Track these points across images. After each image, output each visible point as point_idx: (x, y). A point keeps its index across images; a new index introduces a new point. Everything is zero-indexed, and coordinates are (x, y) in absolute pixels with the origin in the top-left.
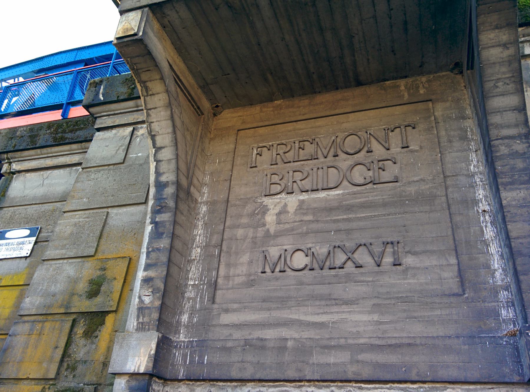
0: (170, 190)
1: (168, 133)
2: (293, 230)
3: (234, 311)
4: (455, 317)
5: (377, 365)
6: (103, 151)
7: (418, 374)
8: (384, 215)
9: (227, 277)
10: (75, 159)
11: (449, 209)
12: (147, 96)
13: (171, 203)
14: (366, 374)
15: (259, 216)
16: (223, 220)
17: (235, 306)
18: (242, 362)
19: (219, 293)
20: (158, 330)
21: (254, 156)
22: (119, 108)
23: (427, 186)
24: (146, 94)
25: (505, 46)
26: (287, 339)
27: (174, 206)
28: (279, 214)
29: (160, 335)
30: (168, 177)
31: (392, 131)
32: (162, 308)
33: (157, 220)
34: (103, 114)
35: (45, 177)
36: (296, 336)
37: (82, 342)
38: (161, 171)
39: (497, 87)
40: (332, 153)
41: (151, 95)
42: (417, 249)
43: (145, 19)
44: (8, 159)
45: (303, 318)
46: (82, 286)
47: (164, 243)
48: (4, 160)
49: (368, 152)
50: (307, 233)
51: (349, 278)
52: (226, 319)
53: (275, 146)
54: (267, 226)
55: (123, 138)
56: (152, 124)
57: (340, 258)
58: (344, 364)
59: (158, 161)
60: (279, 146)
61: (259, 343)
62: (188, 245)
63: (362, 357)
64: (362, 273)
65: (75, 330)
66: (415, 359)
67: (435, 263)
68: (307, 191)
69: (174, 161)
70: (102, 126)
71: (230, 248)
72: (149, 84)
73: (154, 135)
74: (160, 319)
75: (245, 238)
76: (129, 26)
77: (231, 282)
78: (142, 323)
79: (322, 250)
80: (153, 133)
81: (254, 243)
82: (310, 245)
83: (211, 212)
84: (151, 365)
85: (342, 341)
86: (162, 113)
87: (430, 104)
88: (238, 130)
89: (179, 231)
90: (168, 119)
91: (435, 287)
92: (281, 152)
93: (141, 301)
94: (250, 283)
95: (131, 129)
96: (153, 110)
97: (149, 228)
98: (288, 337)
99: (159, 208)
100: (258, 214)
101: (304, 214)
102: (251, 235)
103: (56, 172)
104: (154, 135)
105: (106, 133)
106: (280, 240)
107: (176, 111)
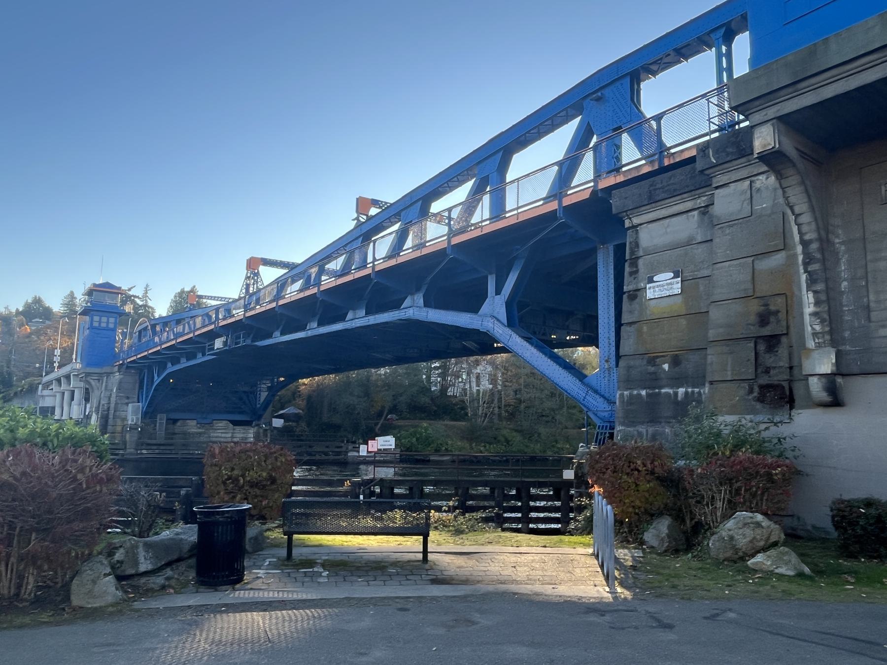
0: (814, 246)
12: (782, 179)
13: (818, 256)
22: (731, 166)
24: (779, 178)
32: (831, 332)
33: (809, 269)
34: (717, 173)
35: (666, 226)
37: (767, 356)
38: (804, 232)
44: (628, 215)
46: (753, 318)
55: (743, 192)
65: (758, 347)
69: (813, 223)
72: (783, 172)
78: (819, 343)
84: (834, 368)
86: (797, 189)
90: (803, 193)
93: (813, 329)
95: (747, 183)
97: (804, 277)
99: (808, 260)
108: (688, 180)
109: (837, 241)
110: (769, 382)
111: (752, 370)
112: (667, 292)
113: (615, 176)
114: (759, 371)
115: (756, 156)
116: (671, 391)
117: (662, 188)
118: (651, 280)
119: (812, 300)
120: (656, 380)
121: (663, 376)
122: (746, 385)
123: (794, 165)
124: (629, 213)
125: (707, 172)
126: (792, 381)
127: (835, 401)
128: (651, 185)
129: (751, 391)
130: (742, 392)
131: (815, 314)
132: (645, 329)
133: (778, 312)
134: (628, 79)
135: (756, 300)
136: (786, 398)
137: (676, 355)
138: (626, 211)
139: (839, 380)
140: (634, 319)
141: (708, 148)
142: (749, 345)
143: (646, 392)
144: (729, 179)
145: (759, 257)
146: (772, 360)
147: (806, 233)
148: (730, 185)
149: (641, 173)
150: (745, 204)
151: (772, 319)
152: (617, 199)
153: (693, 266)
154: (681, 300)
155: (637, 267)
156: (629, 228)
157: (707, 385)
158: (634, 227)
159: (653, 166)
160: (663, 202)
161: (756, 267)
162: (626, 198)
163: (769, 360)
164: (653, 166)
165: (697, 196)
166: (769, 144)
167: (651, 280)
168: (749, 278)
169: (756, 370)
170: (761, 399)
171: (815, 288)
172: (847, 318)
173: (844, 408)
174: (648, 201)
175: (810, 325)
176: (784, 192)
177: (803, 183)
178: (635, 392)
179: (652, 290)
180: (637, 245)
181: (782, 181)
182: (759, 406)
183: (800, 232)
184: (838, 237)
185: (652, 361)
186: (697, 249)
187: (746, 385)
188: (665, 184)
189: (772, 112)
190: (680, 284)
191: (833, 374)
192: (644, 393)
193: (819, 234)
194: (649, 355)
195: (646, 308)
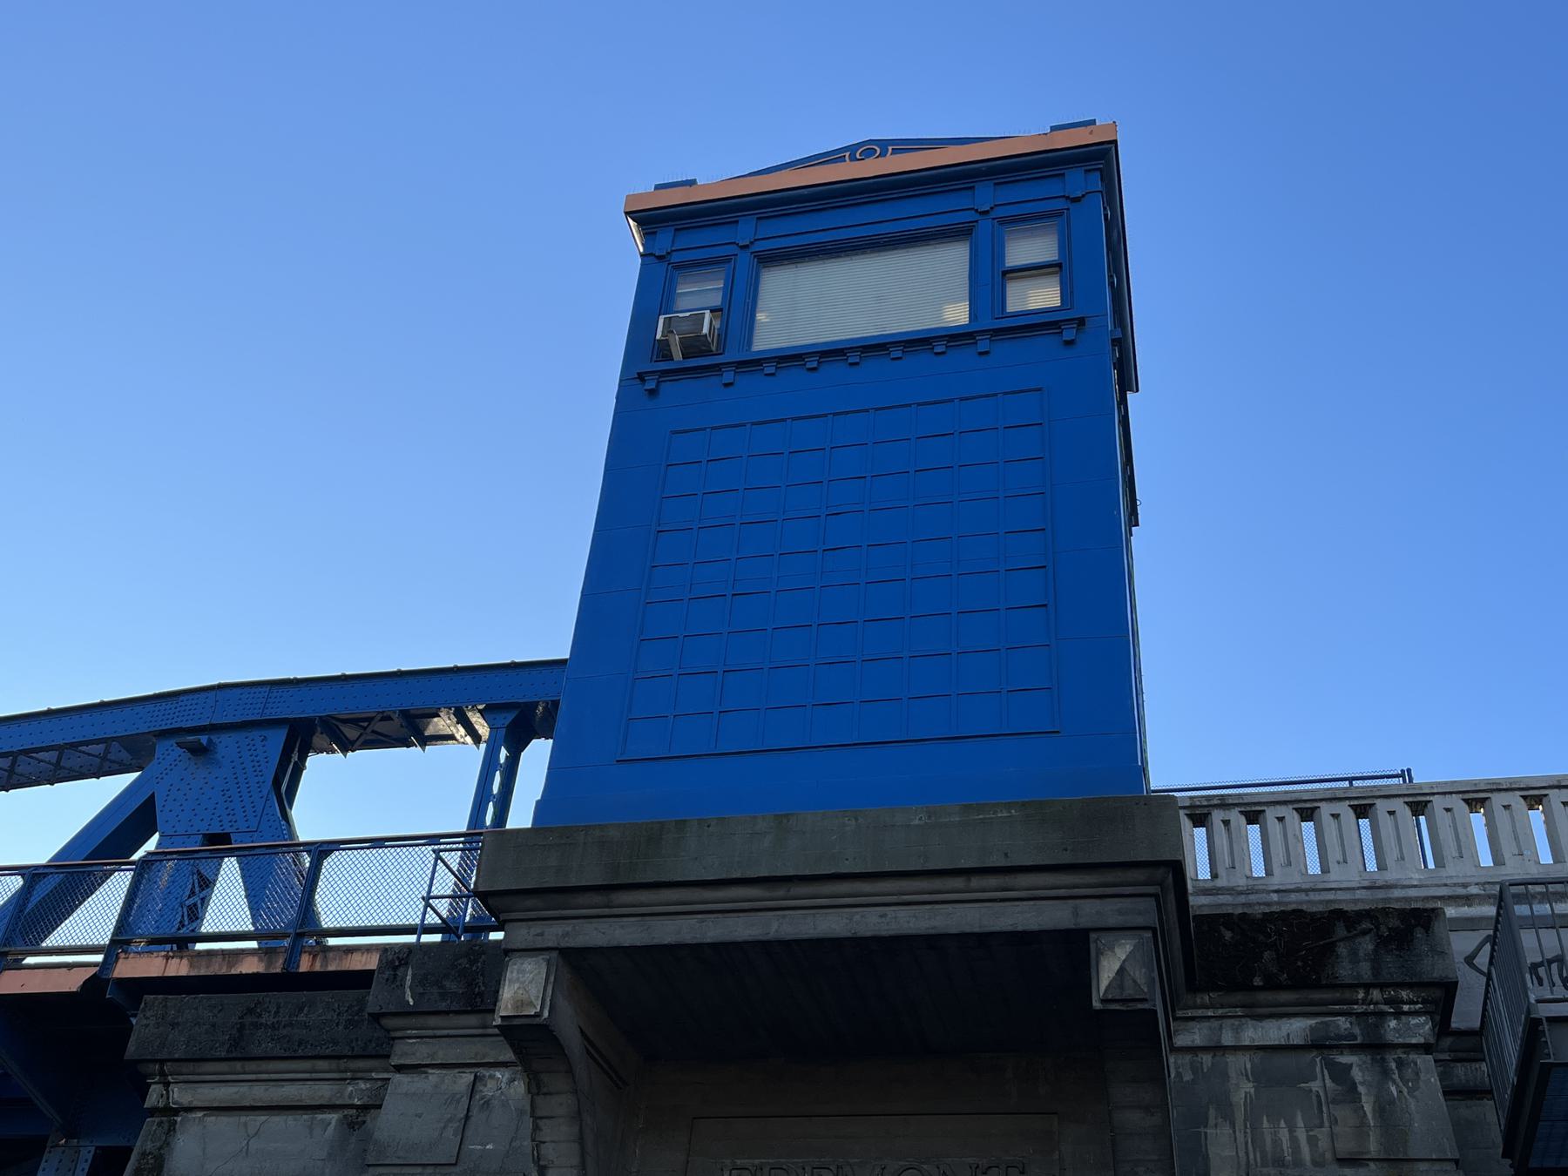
1: (571, 1167)
6: (411, 1128)
12: (538, 1094)
24: (534, 1090)
35: (251, 1131)
41: (545, 1094)
43: (552, 979)
48: (152, 1075)
53: (766, 1170)
56: (542, 1146)
60: (773, 1171)
70: (408, 1062)
76: (525, 997)
80: (542, 1163)
95: (468, 1077)
96: (544, 1120)
103: (277, 1121)
105: (416, 1079)
115: (498, 1022)
117: (273, 1027)
125: (386, 1022)
128: (250, 1011)
134: (279, 737)
138: (162, 1062)
141: (407, 964)
149: (233, 972)
150: (449, 1133)
156: (153, 1111)
158: (170, 1112)
164: (269, 964)
176: (536, 1128)
181: (539, 1100)
189: (554, 933)
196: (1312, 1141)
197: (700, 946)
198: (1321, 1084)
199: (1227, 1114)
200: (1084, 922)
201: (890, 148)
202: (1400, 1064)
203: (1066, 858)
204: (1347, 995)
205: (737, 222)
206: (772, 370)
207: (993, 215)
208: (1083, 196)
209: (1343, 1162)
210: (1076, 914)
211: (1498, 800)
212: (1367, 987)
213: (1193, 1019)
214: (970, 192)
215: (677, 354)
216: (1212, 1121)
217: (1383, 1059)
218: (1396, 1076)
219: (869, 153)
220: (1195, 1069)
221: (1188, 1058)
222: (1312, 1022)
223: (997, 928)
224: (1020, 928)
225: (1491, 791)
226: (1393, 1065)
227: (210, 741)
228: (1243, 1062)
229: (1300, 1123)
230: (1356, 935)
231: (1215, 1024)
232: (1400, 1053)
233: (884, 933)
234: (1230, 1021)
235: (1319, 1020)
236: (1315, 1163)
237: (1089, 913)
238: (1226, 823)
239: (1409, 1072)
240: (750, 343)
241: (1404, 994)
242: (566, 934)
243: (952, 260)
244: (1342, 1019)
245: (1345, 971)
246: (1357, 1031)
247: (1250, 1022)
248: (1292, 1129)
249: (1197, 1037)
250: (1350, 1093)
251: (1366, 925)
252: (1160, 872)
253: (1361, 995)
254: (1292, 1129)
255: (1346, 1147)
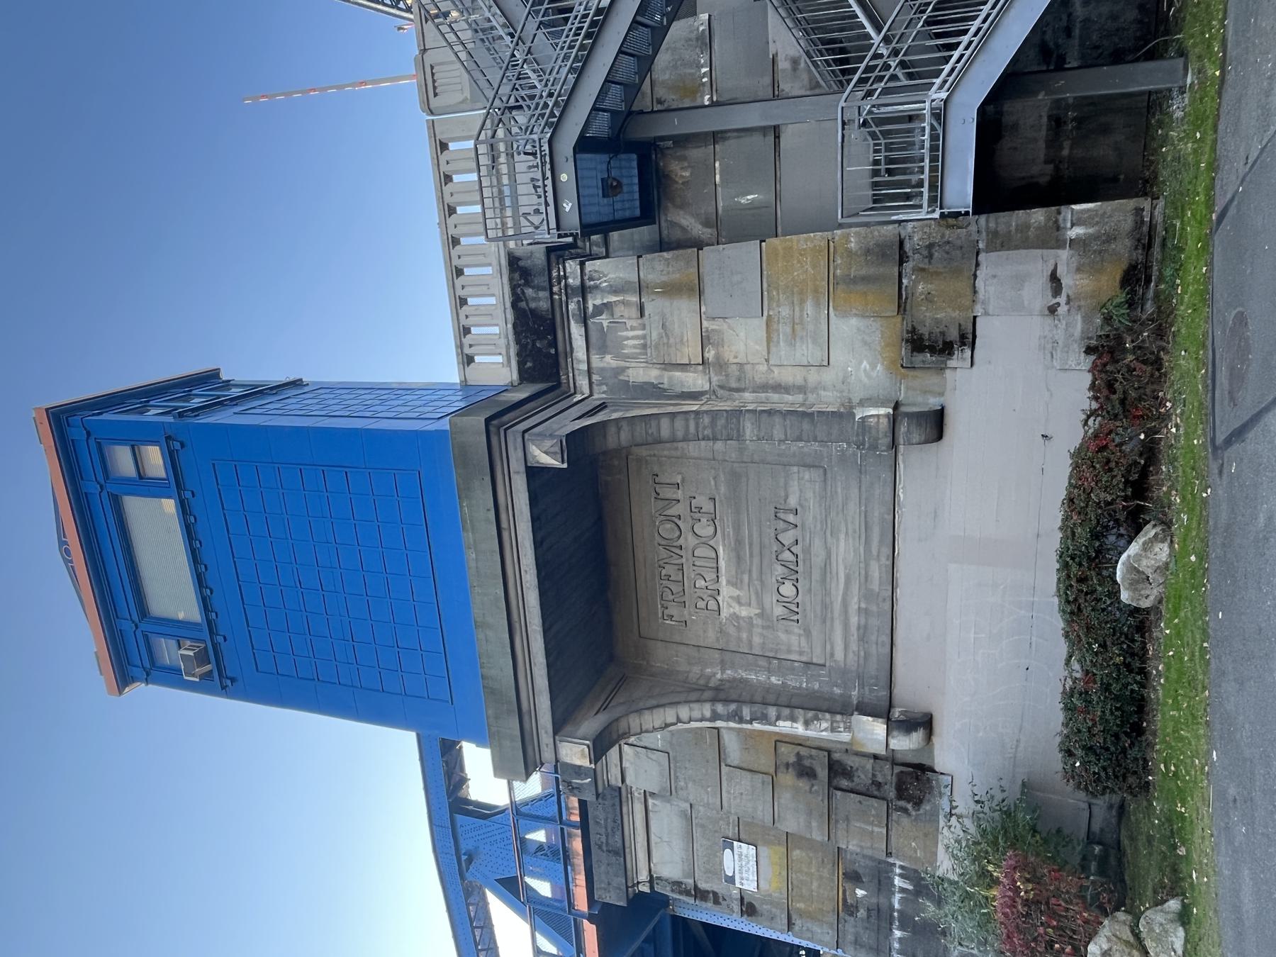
0: (720, 708)
2: (757, 593)
3: (832, 648)
4: (844, 478)
5: (881, 542)
7: (889, 514)
8: (748, 514)
9: (801, 653)
10: (639, 808)
11: (746, 463)
13: (733, 707)
14: (887, 551)
15: (741, 622)
16: (742, 655)
17: (828, 647)
18: (877, 644)
19: (815, 660)
20: (852, 715)
21: (673, 623)
23: (722, 476)
25: (619, 429)
26: (859, 608)
27: (736, 704)
28: (740, 603)
29: (856, 713)
30: (707, 710)
31: (659, 494)
32: (832, 712)
33: (748, 719)
34: (605, 777)
35: (659, 840)
36: (856, 599)
38: (700, 716)
39: (652, 433)
40: (677, 551)
42: (783, 494)
43: (570, 739)
45: (841, 593)
46: (803, 784)
47: (772, 711)
49: (680, 519)
50: (762, 581)
51: (807, 551)
52: (839, 655)
53: (663, 602)
54: (752, 615)
55: (637, 754)
57: (787, 555)
58: (880, 567)
59: (690, 720)
61: (861, 631)
62: (769, 689)
63: (875, 552)
64: (803, 540)
65: (844, 787)
66: (876, 514)
67: (796, 483)
68: (718, 577)
69: (692, 705)
71: (771, 650)
72: (621, 732)
73: (666, 724)
74: (842, 714)
75: (762, 635)
77: (806, 650)
78: (845, 728)
79: (780, 570)
81: (768, 627)
82: (774, 580)
83: (733, 667)
84: (880, 720)
85: (862, 565)
87: (630, 457)
88: (640, 636)
89: (758, 698)
91: (817, 487)
92: (671, 597)
93: (825, 730)
94: (808, 633)
97: (757, 726)
98: (856, 607)
99: (737, 718)
100: (739, 623)
101: (741, 582)
102: (760, 630)
104: (666, 724)
106: (767, 606)
107: (641, 705)
108: (606, 803)
109: (719, 676)
110: (894, 785)
111: (874, 802)
112: (751, 863)
113: (576, 886)
114: (876, 793)
115: (593, 766)
116: (898, 896)
117: (607, 836)
118: (731, 880)
119: (788, 724)
120: (879, 910)
121: (874, 900)
122: (895, 815)
123: (617, 720)
124: (630, 885)
125: (600, 790)
126: (893, 760)
127: (924, 723)
128: (600, 847)
129: (905, 811)
130: (905, 821)
131: (807, 724)
132: (801, 905)
133: (798, 754)
134: (459, 817)
135: (779, 775)
136: (916, 773)
137: (844, 874)
138: (627, 887)
139: (896, 713)
140: (784, 916)
141: (571, 782)
142: (838, 797)
143: (897, 929)
144: (616, 766)
145: (722, 756)
146: (863, 776)
147: (702, 714)
148: (623, 766)
149: (581, 852)
150: (654, 757)
151: (807, 763)
152: (608, 895)
153: (721, 822)
154: (765, 848)
155: (708, 892)
156: (652, 887)
157: (891, 860)
158: (651, 881)
159: (576, 835)
160: (627, 838)
161: (736, 763)
162: (609, 884)
163: (862, 779)
164: (576, 835)
165: (629, 796)
166: (583, 750)
167: (731, 880)
168: (748, 775)
169: (875, 797)
170: (918, 803)
171: (774, 718)
172: (817, 686)
173: (933, 714)
174: (620, 857)
175: (821, 731)
176: (647, 731)
177: (639, 711)
178: (896, 945)
179: (744, 882)
180: (679, 883)
181: (632, 732)
182: (926, 807)
183: (701, 720)
184: (714, 674)
185: (850, 908)
186: (699, 812)
187: (895, 815)
188: (604, 830)
189: (546, 738)
190: (742, 844)
191: (888, 721)
192: (898, 934)
193: (705, 701)
194: (840, 909)
195: (770, 895)
196: (633, 329)
197: (548, 666)
198: (604, 320)
199: (624, 369)
200: (523, 469)
201: (64, 539)
202: (591, 279)
203: (488, 479)
204: (557, 304)
205: (120, 630)
206: (214, 614)
207: (103, 482)
208: (85, 429)
209: (642, 315)
210: (518, 473)
211: (448, 199)
212: (552, 293)
213: (574, 383)
214: (89, 496)
215: (208, 667)
216: (627, 379)
217: (590, 287)
218: (598, 282)
219: (67, 552)
220: (600, 384)
221: (595, 387)
222: (572, 322)
223: (529, 514)
224: (528, 502)
225: (443, 202)
226: (592, 283)
227: (465, 854)
228: (595, 359)
229: (625, 334)
230: (525, 297)
231: (576, 372)
232: (586, 278)
233: (536, 571)
234: (575, 366)
235: (571, 318)
236: (644, 328)
237: (517, 465)
238: (471, 346)
239: (595, 275)
240: (196, 624)
241: (555, 274)
242: (546, 732)
243: (135, 506)
244: (570, 307)
245: (544, 305)
246: (575, 300)
247: (574, 354)
248: (628, 338)
249: (584, 383)
250: (607, 307)
251: (519, 290)
252: (492, 429)
253: (557, 297)
254: (628, 338)
255: (634, 312)
